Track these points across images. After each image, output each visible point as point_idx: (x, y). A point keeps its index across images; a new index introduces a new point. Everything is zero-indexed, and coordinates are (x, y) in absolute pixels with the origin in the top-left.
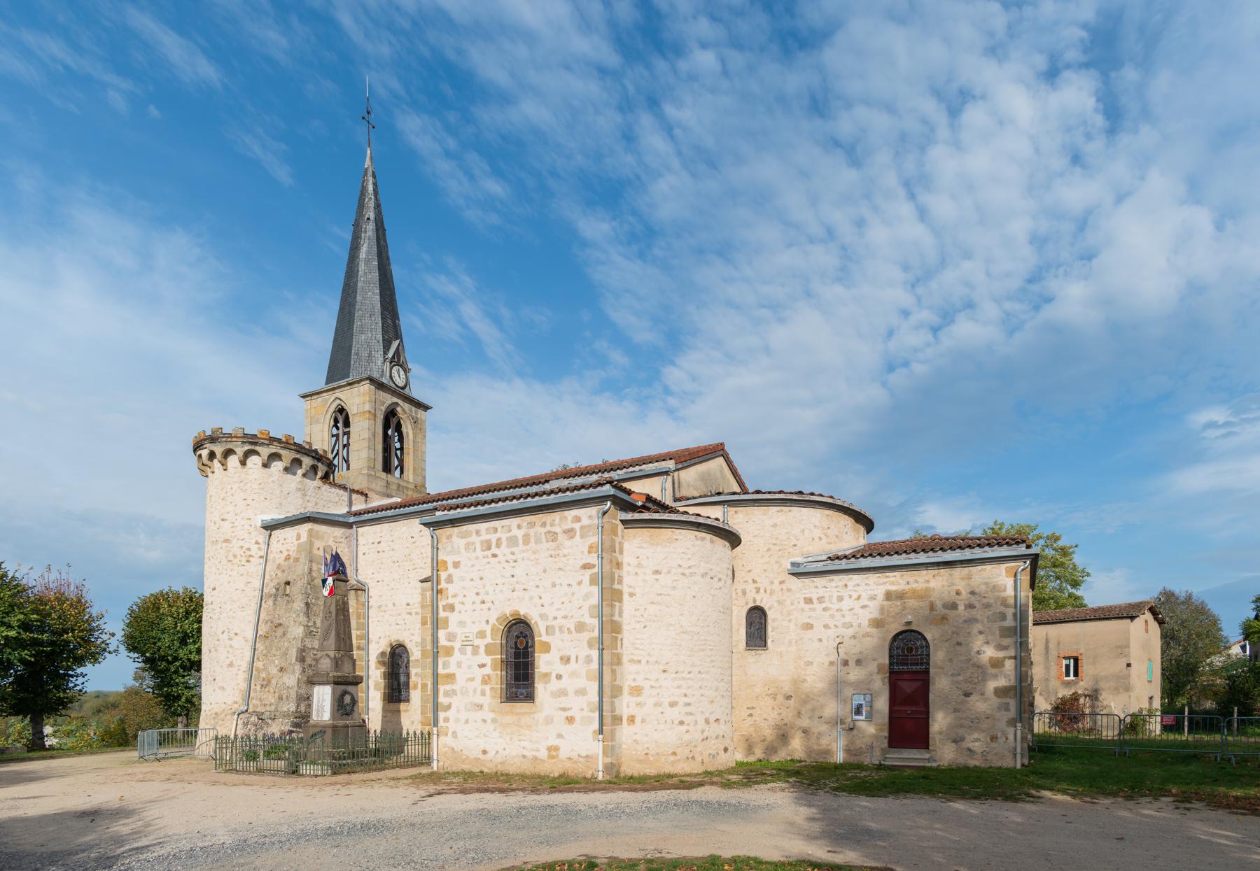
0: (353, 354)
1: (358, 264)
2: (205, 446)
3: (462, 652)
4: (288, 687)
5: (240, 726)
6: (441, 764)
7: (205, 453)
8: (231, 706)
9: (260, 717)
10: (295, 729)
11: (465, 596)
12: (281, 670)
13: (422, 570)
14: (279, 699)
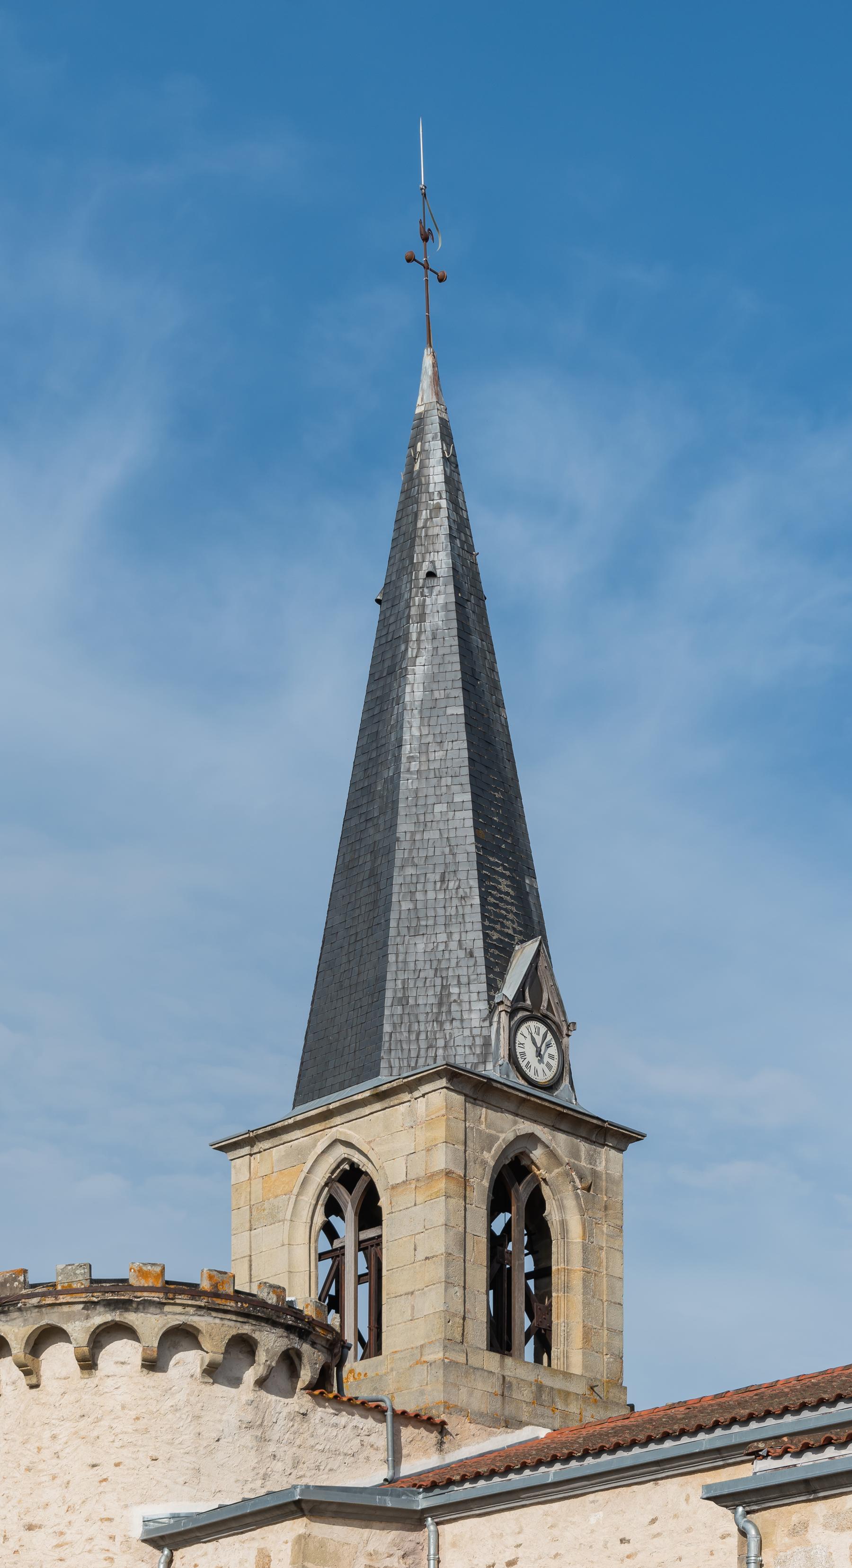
0: (388, 1002)
1: (399, 726)
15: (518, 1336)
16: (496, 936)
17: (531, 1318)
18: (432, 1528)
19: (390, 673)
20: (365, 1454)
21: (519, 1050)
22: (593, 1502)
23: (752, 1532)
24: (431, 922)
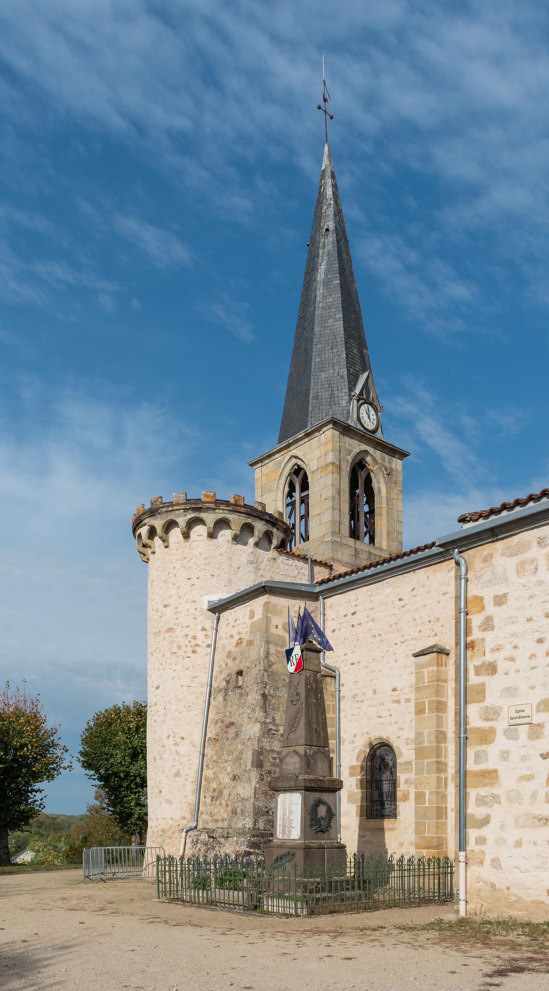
0: (311, 398)
1: (315, 290)
2: (144, 522)
3: (511, 734)
4: (243, 799)
5: (189, 845)
6: (471, 906)
7: (144, 531)
8: (179, 821)
9: (211, 835)
10: (252, 850)
11: (515, 647)
12: (234, 778)
13: (414, 642)
14: (233, 813)
15: (362, 534)
16: (352, 370)
17: (367, 528)
18: (322, 600)
19: (312, 271)
20: (300, 577)
21: (361, 416)
22: (387, 583)
23: (463, 562)
24: (327, 366)
